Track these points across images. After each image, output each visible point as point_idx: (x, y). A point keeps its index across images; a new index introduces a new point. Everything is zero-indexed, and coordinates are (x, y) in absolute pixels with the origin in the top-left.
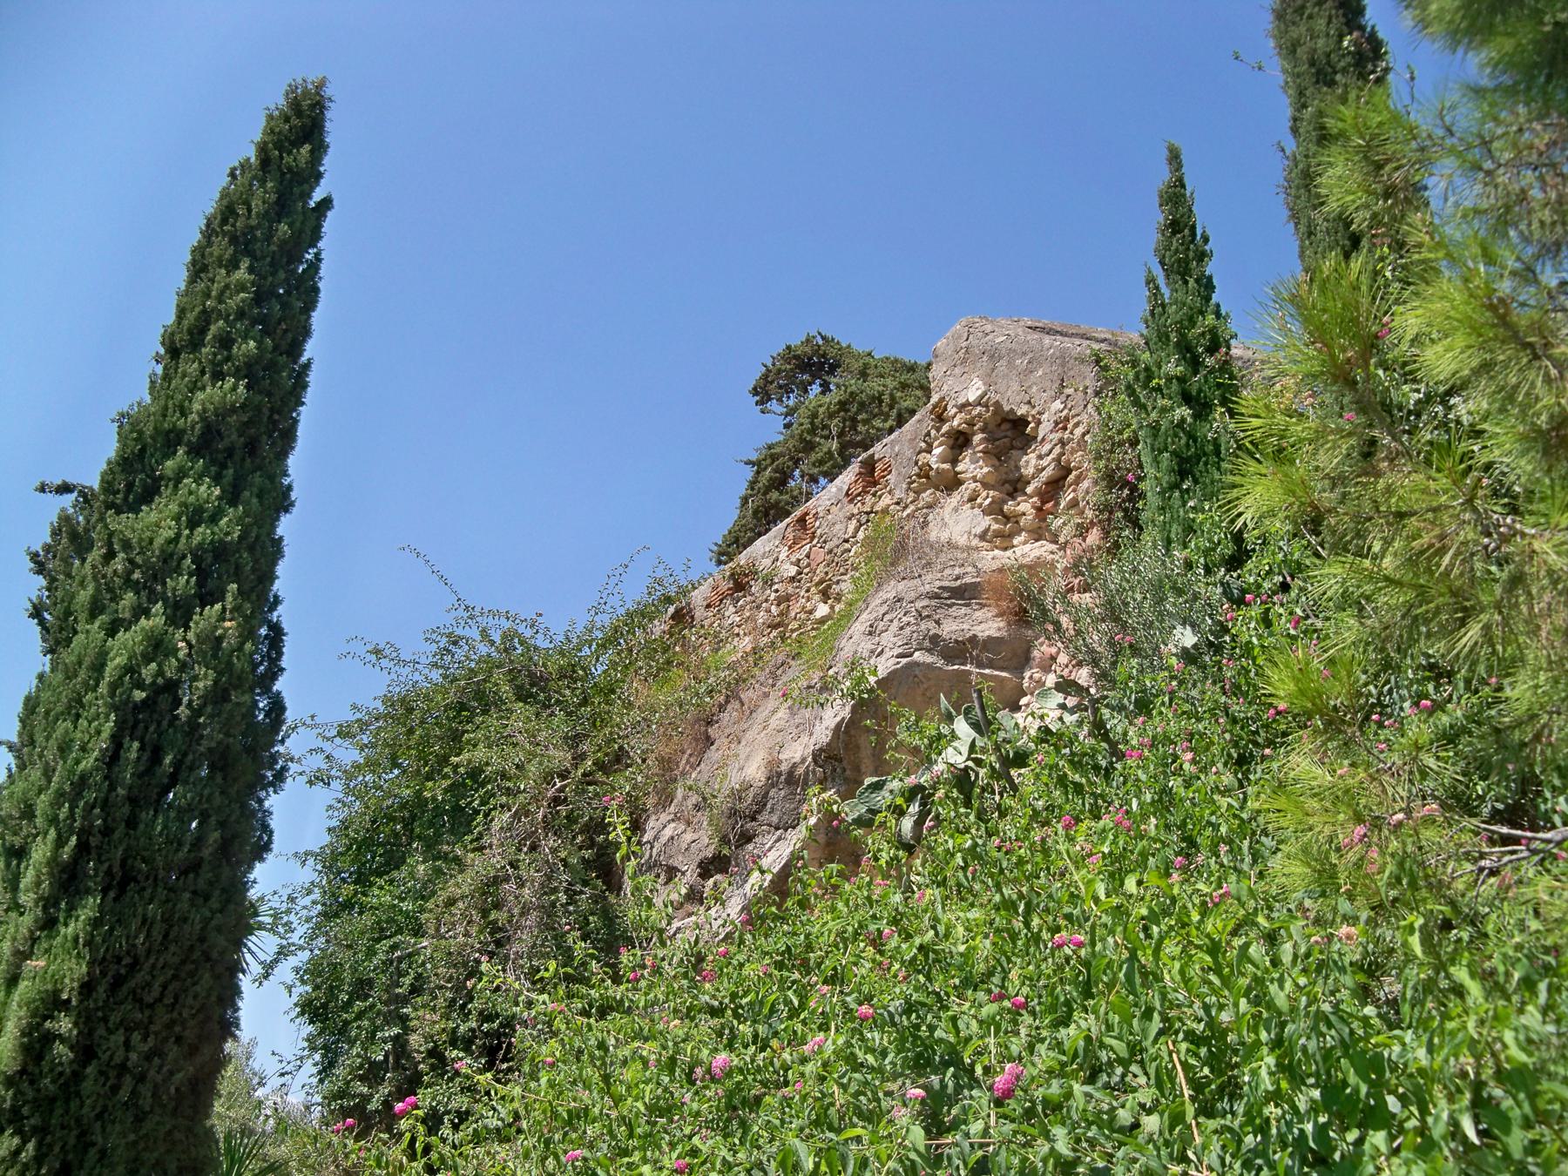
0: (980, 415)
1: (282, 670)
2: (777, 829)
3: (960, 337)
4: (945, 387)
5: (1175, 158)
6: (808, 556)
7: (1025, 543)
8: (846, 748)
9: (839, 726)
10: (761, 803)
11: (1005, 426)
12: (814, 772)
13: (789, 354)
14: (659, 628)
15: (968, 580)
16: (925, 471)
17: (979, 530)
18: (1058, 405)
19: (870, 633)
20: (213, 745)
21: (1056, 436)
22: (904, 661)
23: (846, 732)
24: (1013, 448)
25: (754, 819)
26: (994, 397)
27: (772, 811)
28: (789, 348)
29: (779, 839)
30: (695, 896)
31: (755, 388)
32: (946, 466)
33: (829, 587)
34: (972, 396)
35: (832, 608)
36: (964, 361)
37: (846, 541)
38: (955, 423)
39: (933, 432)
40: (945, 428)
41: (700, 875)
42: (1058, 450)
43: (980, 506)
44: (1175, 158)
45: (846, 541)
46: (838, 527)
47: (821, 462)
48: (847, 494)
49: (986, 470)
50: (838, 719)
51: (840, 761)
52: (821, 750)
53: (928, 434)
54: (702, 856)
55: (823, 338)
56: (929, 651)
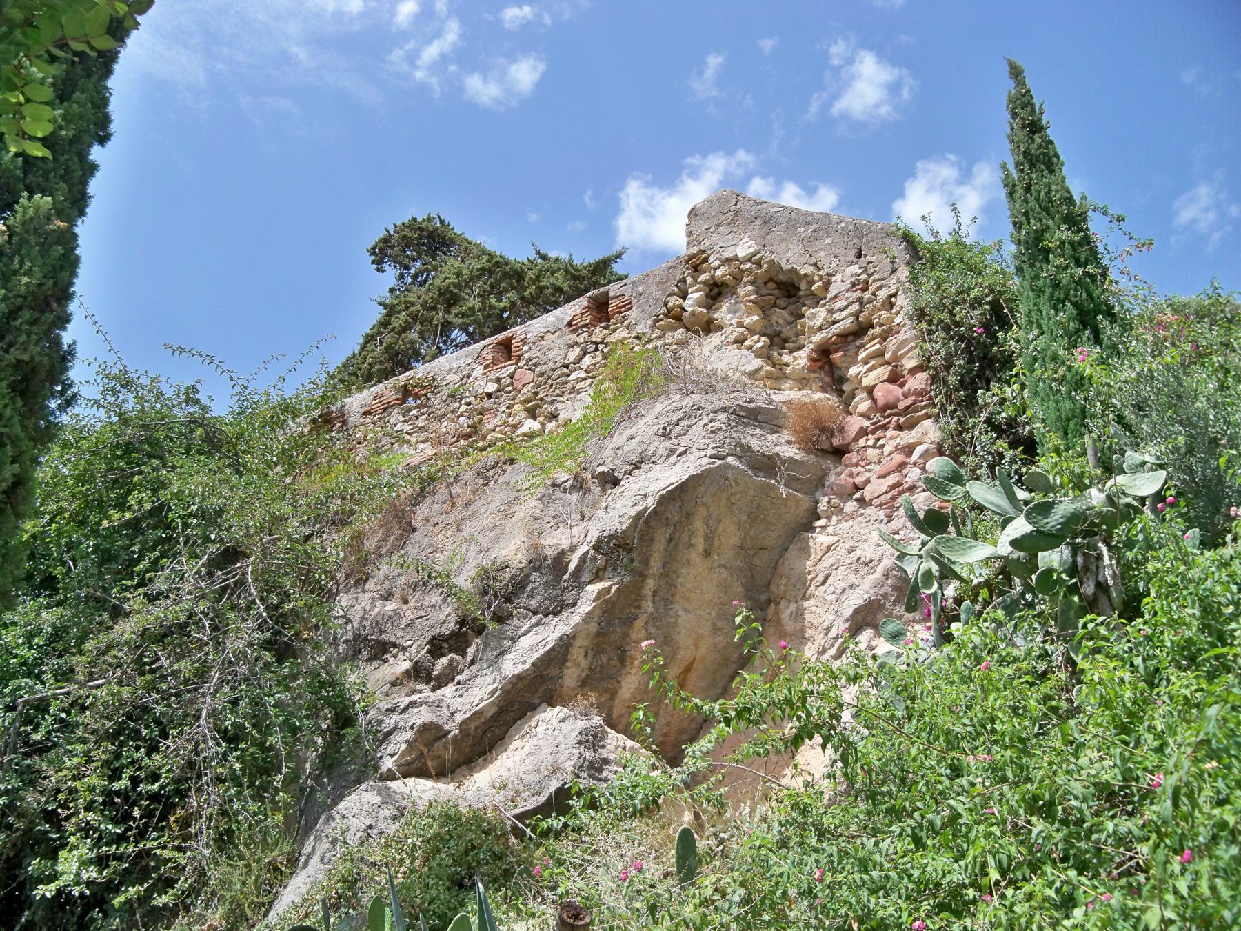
0: (750, 271)
1: (71, 314)
2: (535, 613)
3: (727, 201)
4: (707, 243)
5: (1016, 73)
6: (511, 376)
7: (791, 389)
8: (641, 539)
9: (639, 515)
10: (519, 585)
11: (771, 285)
12: (594, 560)
13: (413, 225)
14: (299, 426)
15: (760, 404)
16: (676, 317)
17: (749, 369)
18: (855, 269)
19: (664, 435)
20: (26, 357)
21: (854, 296)
22: (719, 462)
23: (647, 522)
24: (775, 305)
25: (508, 600)
26: (767, 256)
27: (531, 596)
28: (414, 219)
29: (538, 624)
30: (419, 673)
31: (374, 248)
32: (704, 310)
33: (537, 406)
34: (742, 251)
35: (543, 425)
36: (732, 222)
37: (567, 366)
38: (719, 273)
39: (689, 280)
40: (703, 277)
41: (429, 652)
42: (856, 307)
43: (750, 348)
44: (1016, 73)
45: (567, 366)
46: (555, 352)
47: (463, 315)
48: (570, 324)
49: (756, 318)
50: (638, 508)
51: (630, 551)
52: (612, 537)
53: (683, 280)
54: (434, 632)
55: (442, 222)
56: (739, 457)
